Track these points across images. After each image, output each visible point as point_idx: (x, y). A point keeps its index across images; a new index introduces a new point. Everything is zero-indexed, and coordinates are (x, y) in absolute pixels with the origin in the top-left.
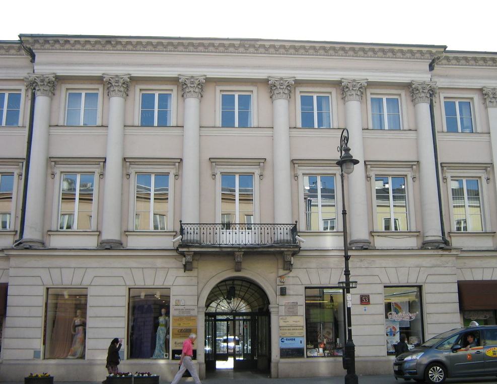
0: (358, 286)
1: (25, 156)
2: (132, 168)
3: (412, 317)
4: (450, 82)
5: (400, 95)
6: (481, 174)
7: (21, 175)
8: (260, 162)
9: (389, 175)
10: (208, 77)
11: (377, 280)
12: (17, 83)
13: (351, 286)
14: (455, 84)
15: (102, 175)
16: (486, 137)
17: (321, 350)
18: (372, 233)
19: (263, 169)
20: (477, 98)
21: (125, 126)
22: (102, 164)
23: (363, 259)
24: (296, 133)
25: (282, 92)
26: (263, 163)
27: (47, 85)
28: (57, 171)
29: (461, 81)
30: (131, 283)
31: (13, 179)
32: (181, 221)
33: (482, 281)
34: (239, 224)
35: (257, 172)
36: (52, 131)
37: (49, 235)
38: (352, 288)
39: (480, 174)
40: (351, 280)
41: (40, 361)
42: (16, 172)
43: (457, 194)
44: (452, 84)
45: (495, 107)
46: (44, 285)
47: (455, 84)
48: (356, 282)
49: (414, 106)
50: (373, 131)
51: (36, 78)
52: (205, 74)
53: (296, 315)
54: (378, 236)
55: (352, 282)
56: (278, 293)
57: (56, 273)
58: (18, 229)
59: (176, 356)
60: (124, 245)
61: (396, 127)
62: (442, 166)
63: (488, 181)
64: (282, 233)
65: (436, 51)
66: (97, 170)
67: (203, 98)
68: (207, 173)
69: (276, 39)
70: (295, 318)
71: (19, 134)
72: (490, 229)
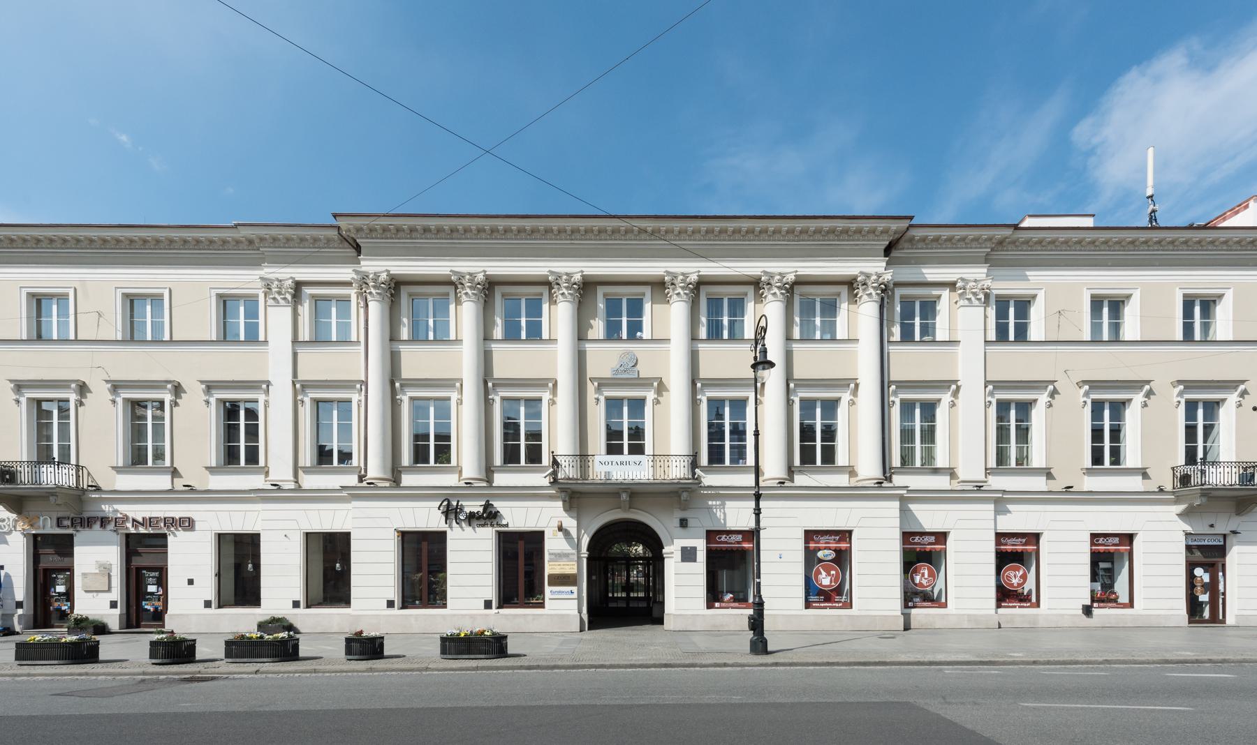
58: (362, 465)
59: (1206, 614)
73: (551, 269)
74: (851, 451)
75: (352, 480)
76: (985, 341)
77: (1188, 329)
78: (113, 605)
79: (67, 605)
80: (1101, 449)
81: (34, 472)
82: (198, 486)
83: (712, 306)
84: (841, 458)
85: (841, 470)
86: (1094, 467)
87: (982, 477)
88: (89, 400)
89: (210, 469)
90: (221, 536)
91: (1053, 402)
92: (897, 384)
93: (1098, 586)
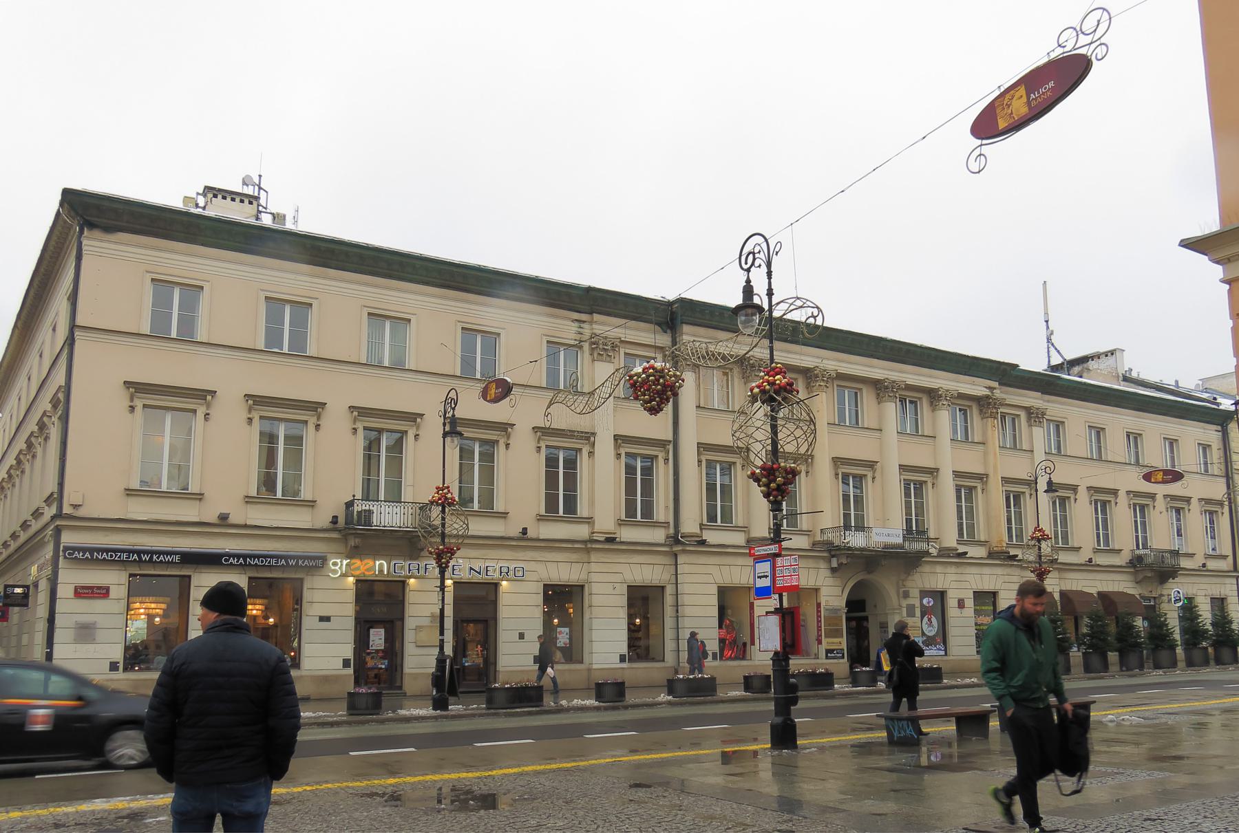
1: (670, 437)
5: (731, 369)
6: (308, 417)
7: (668, 460)
8: (871, 465)
9: (718, 461)
11: (967, 585)
12: (647, 349)
15: (591, 454)
16: (1029, 454)
17: (286, 656)
19: (208, 406)
20: (1023, 415)
21: (984, 444)
28: (139, 404)
30: (720, 581)
35: (312, 421)
41: (120, 675)
42: (661, 456)
49: (879, 404)
50: (1055, 456)
52: (958, 389)
53: (914, 616)
56: (901, 595)
57: (725, 569)
59: (829, 655)
61: (916, 432)
63: (207, 416)
64: (398, 512)
71: (247, 359)
72: (504, 508)
74: (592, 503)
75: (658, 535)
76: (698, 407)
77: (273, 336)
78: (346, 663)
79: (384, 664)
80: (1138, 536)
81: (402, 513)
82: (233, 519)
83: (733, 380)
84: (583, 510)
85: (737, 529)
86: (708, 524)
87: (698, 531)
88: (1224, 515)
89: (249, 500)
90: (187, 579)
91: (1190, 508)
92: (254, 399)
93: (723, 631)
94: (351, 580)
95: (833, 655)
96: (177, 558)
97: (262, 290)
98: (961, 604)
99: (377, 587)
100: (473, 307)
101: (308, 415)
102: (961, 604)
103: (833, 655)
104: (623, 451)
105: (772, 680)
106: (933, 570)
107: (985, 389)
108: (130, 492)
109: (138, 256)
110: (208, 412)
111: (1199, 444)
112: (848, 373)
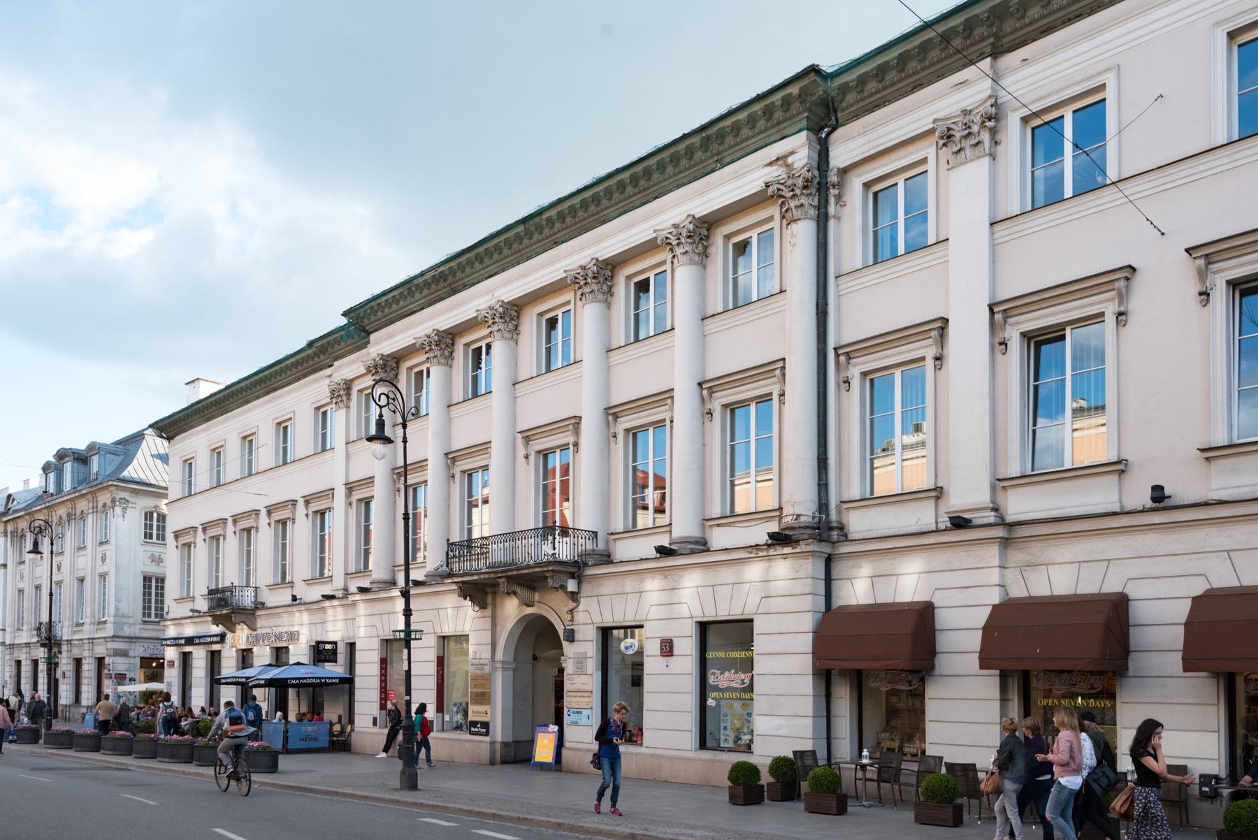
0: (423, 637)
2: (854, 366)
3: (1095, 686)
4: (869, 142)
10: (696, 216)
13: (413, 636)
14: (396, 345)
18: (706, 522)
19: (1122, 297)
20: (928, 150)
22: (778, 372)
23: (668, 573)
24: (618, 357)
25: (690, 251)
26: (1127, 279)
27: (802, 194)
29: (891, 127)
31: (648, 436)
32: (448, 540)
33: (894, 604)
34: (534, 529)
36: (708, 327)
37: (1003, 487)
38: (416, 639)
39: (920, 352)
40: (413, 627)
43: (914, 403)
44: (873, 144)
45: (964, 163)
46: (692, 617)
47: (396, 345)
48: (422, 631)
51: (669, 236)
54: (718, 525)
55: (416, 631)
59: (472, 729)
60: (709, 544)
62: (837, 355)
63: (1121, 318)
65: (801, 89)
66: (927, 350)
67: (709, 259)
68: (521, 451)
69: (770, 87)
70: (584, 679)
73: (415, 336)
94: (234, 649)
95: (476, 730)
96: (183, 641)
97: (1217, 24)
98: (667, 648)
99: (250, 654)
100: (280, 402)
101: (662, 412)
102: (667, 648)
103: (476, 730)
104: (716, 406)
105: (766, 789)
106: (619, 590)
107: (769, 169)
108: (1211, 453)
109: (1114, 44)
110: (1122, 309)
111: (225, 440)
112: (556, 279)
